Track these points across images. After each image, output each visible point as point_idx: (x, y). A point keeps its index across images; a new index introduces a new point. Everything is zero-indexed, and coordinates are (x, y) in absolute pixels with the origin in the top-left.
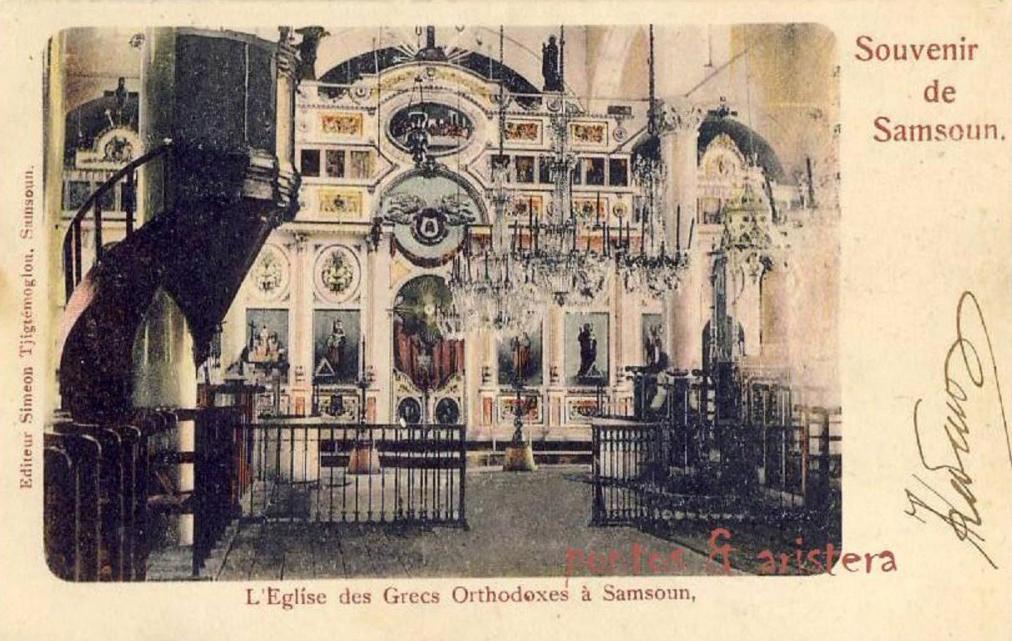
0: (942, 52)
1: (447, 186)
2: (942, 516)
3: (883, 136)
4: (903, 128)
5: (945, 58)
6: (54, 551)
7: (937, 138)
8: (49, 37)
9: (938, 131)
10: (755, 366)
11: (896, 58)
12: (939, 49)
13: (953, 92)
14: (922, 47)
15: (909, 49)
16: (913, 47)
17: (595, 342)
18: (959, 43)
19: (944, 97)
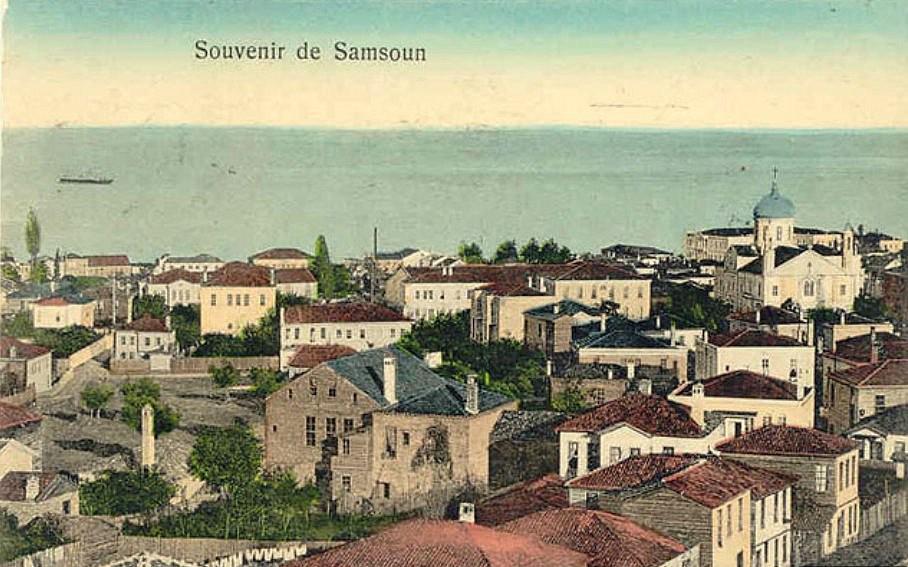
0: (257, 54)
1: (204, 543)
2: (741, 504)
3: (341, 55)
4: (356, 49)
5: (260, 57)
6: (186, 134)
7: (381, 59)
8: (739, 551)
9: (381, 52)
10: (435, 312)
11: (225, 57)
12: (254, 51)
13: (318, 51)
14: (243, 48)
15: (234, 50)
16: (237, 48)
17: (665, 448)
18: (270, 47)
19: (312, 56)
